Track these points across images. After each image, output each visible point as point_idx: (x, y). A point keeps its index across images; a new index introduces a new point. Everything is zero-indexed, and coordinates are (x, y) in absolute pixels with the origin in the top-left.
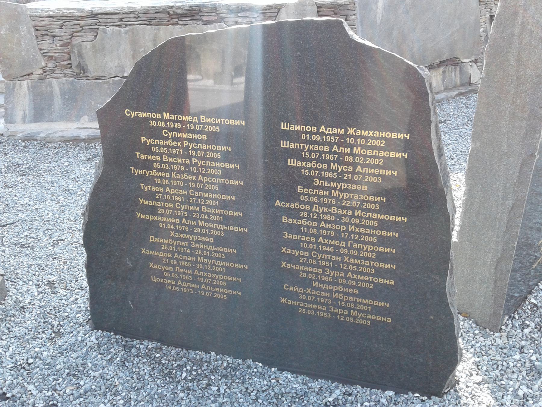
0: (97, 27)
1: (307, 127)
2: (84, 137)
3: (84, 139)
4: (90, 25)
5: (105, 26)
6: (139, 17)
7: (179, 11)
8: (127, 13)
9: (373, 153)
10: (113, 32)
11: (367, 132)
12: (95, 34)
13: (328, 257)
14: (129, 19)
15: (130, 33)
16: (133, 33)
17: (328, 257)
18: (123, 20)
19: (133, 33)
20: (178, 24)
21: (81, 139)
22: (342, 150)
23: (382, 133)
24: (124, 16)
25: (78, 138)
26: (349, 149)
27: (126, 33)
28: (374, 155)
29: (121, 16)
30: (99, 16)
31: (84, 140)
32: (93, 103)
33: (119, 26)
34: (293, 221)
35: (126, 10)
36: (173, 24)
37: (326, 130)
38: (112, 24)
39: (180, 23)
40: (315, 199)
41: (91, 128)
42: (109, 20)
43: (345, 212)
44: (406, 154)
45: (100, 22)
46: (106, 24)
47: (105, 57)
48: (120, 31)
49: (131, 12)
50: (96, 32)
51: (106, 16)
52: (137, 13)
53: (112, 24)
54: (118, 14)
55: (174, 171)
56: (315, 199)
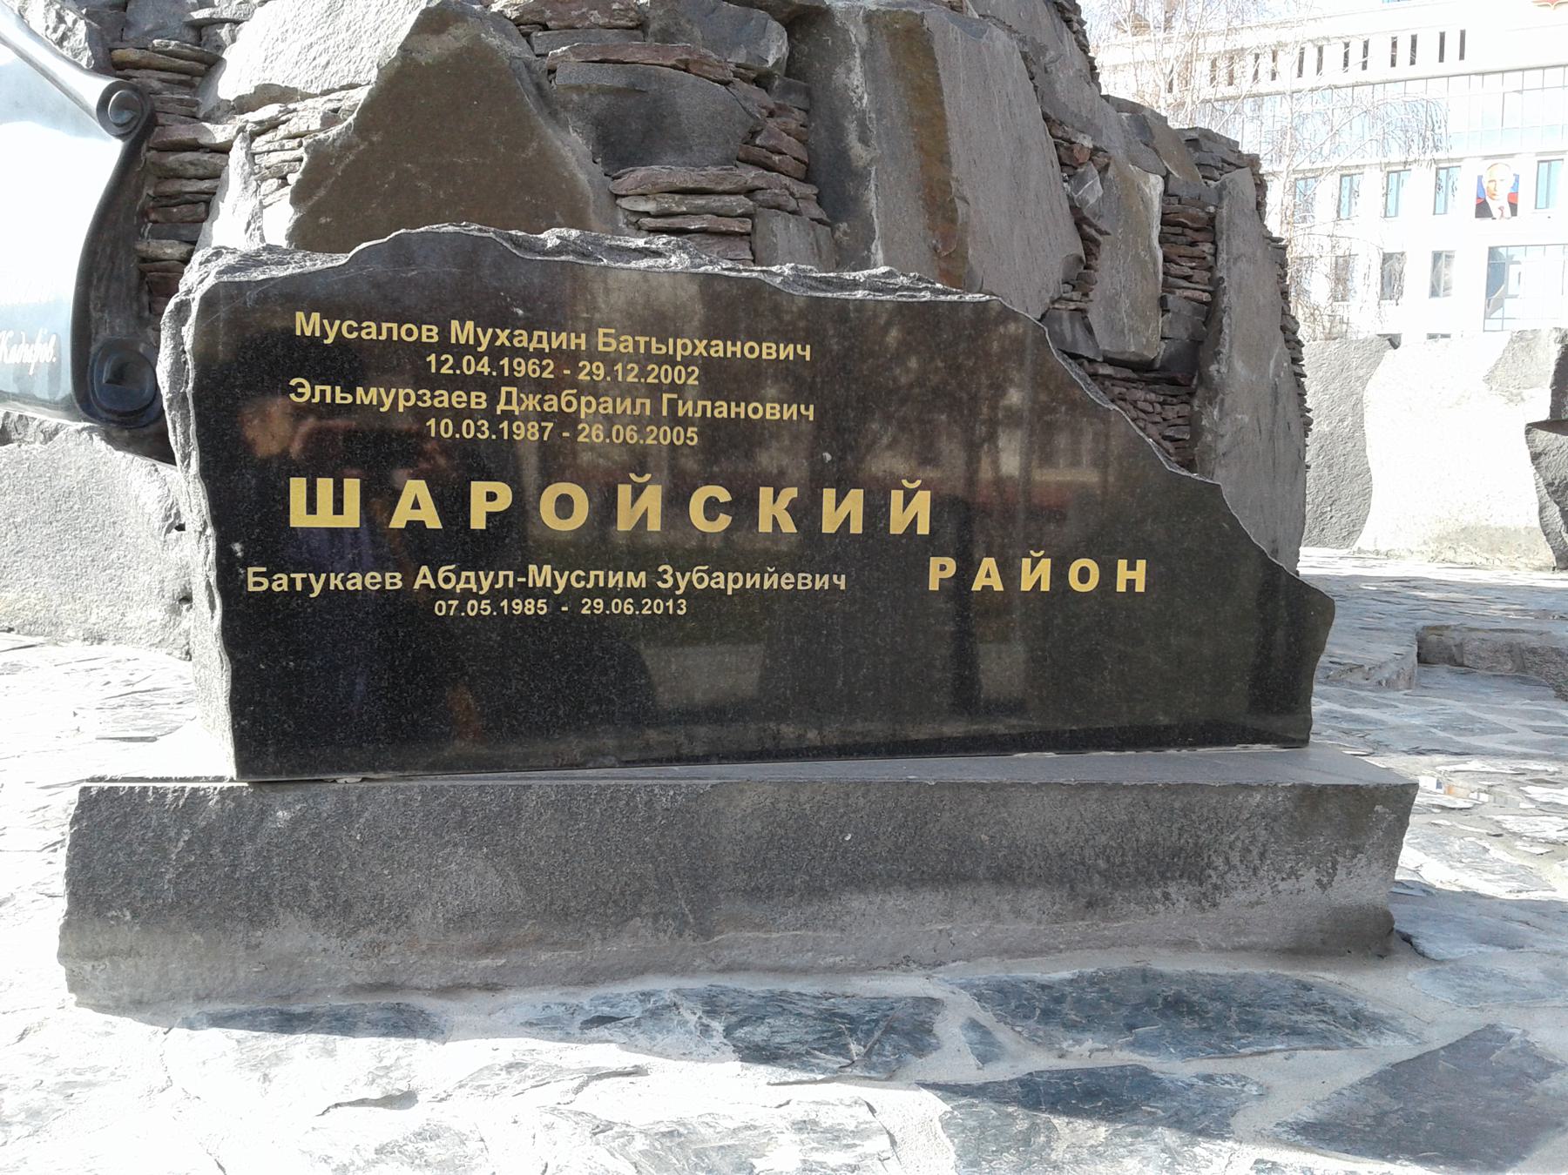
9: (379, 333)
17: (636, 344)
22: (390, 330)
23: (734, 345)
55: (512, 381)
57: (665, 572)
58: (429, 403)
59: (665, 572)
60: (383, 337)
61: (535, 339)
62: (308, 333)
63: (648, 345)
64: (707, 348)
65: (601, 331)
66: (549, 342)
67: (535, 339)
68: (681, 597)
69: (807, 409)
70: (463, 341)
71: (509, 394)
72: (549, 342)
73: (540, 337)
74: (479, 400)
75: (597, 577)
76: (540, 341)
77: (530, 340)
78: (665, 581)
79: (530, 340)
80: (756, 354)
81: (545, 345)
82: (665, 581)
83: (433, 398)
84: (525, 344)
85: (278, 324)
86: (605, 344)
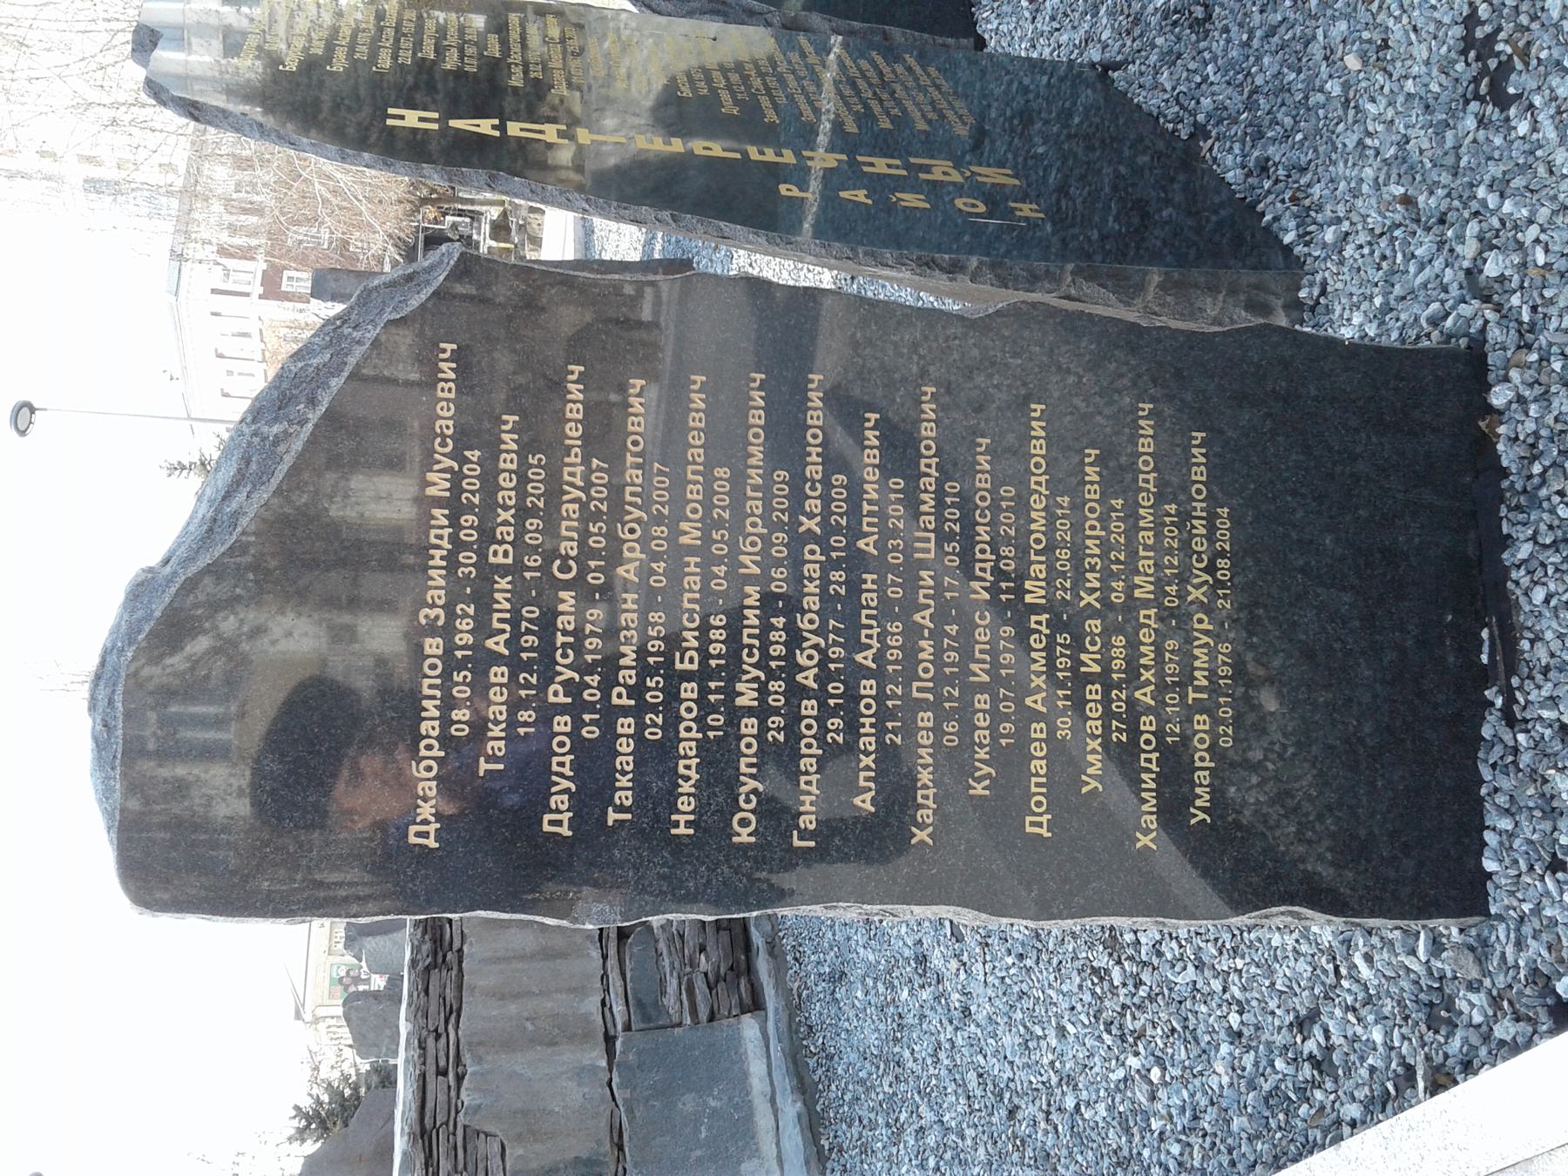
0: (460, 1132)
1: (810, 439)
2: (799, 1104)
3: (805, 1103)
4: (455, 1148)
5: (457, 1112)
6: (436, 1030)
7: (426, 947)
8: (424, 1055)
10: (477, 1089)
11: (1090, 758)
12: (482, 1136)
13: (870, 514)
14: (442, 1054)
15: (481, 1050)
16: (481, 1043)
17: (870, 514)
18: (442, 1063)
19: (481, 1043)
20: (460, 950)
21: (804, 1111)
23: (863, 725)
24: (430, 1061)
25: (805, 1120)
26: (924, 574)
27: (479, 1060)
28: (575, 535)
29: (431, 1070)
30: (428, 1121)
31: (809, 1104)
32: (698, 1153)
33: (460, 1079)
34: (505, 523)
35: (417, 1053)
36: (460, 962)
37: (870, 647)
38: (453, 1093)
39: (456, 945)
40: (468, 558)
41: (778, 1144)
42: (442, 1098)
43: (505, 515)
44: (571, 367)
45: (447, 1123)
46: (454, 1108)
47: (551, 1112)
48: (474, 1074)
49: (422, 1046)
50: (471, 1134)
51: (430, 1105)
52: (424, 1033)
53: (453, 1093)
54: (423, 1076)
56: (468, 558)
57: (426, 616)
58: (441, 612)
59: (426, 616)
60: (872, 785)
61: (438, 542)
62: (448, 485)
63: (870, 502)
64: (867, 754)
65: (678, 666)
66: (442, 527)
67: (438, 542)
68: (826, 640)
69: (695, 382)
70: (448, 485)
71: (551, 823)
72: (442, 527)
73: (1146, 760)
74: (689, 690)
75: (749, 636)
76: (440, 537)
77: (928, 475)
78: (437, 618)
79: (928, 475)
80: (692, 704)
81: (988, 565)
82: (437, 618)
83: (627, 628)
84: (932, 480)
85: (818, 363)
86: (691, 661)
